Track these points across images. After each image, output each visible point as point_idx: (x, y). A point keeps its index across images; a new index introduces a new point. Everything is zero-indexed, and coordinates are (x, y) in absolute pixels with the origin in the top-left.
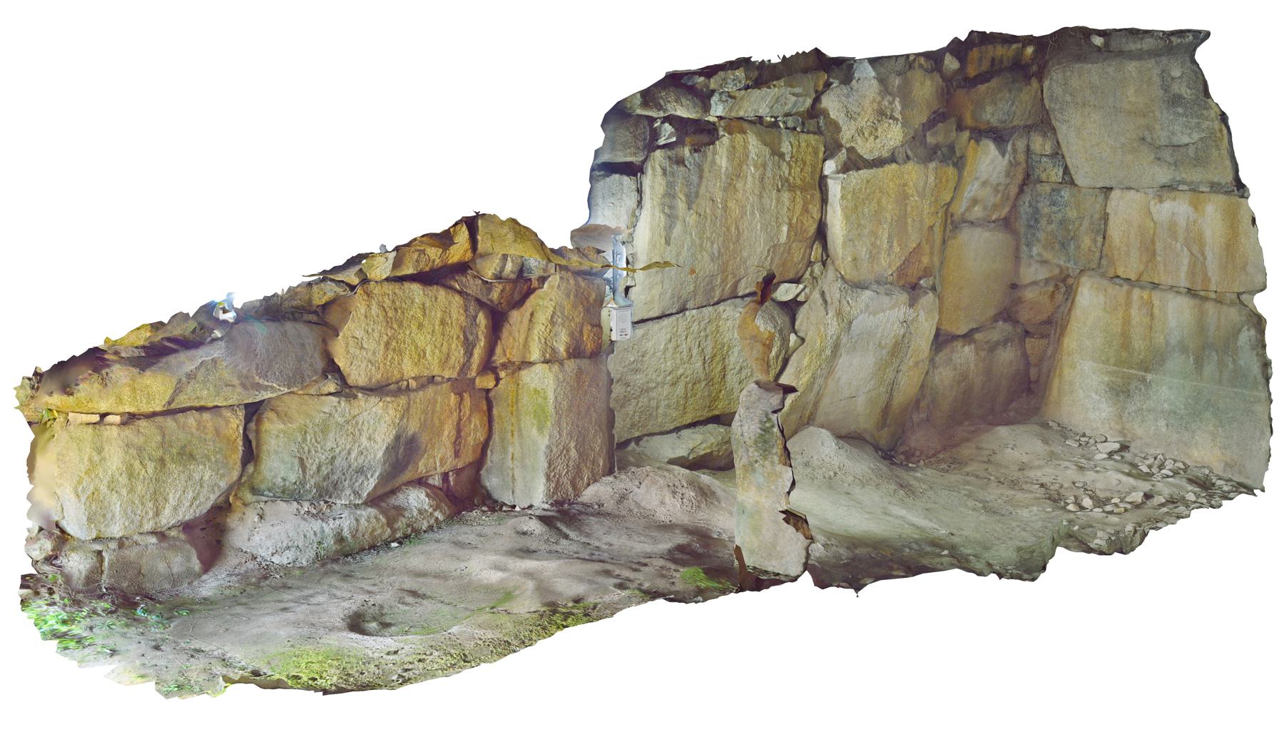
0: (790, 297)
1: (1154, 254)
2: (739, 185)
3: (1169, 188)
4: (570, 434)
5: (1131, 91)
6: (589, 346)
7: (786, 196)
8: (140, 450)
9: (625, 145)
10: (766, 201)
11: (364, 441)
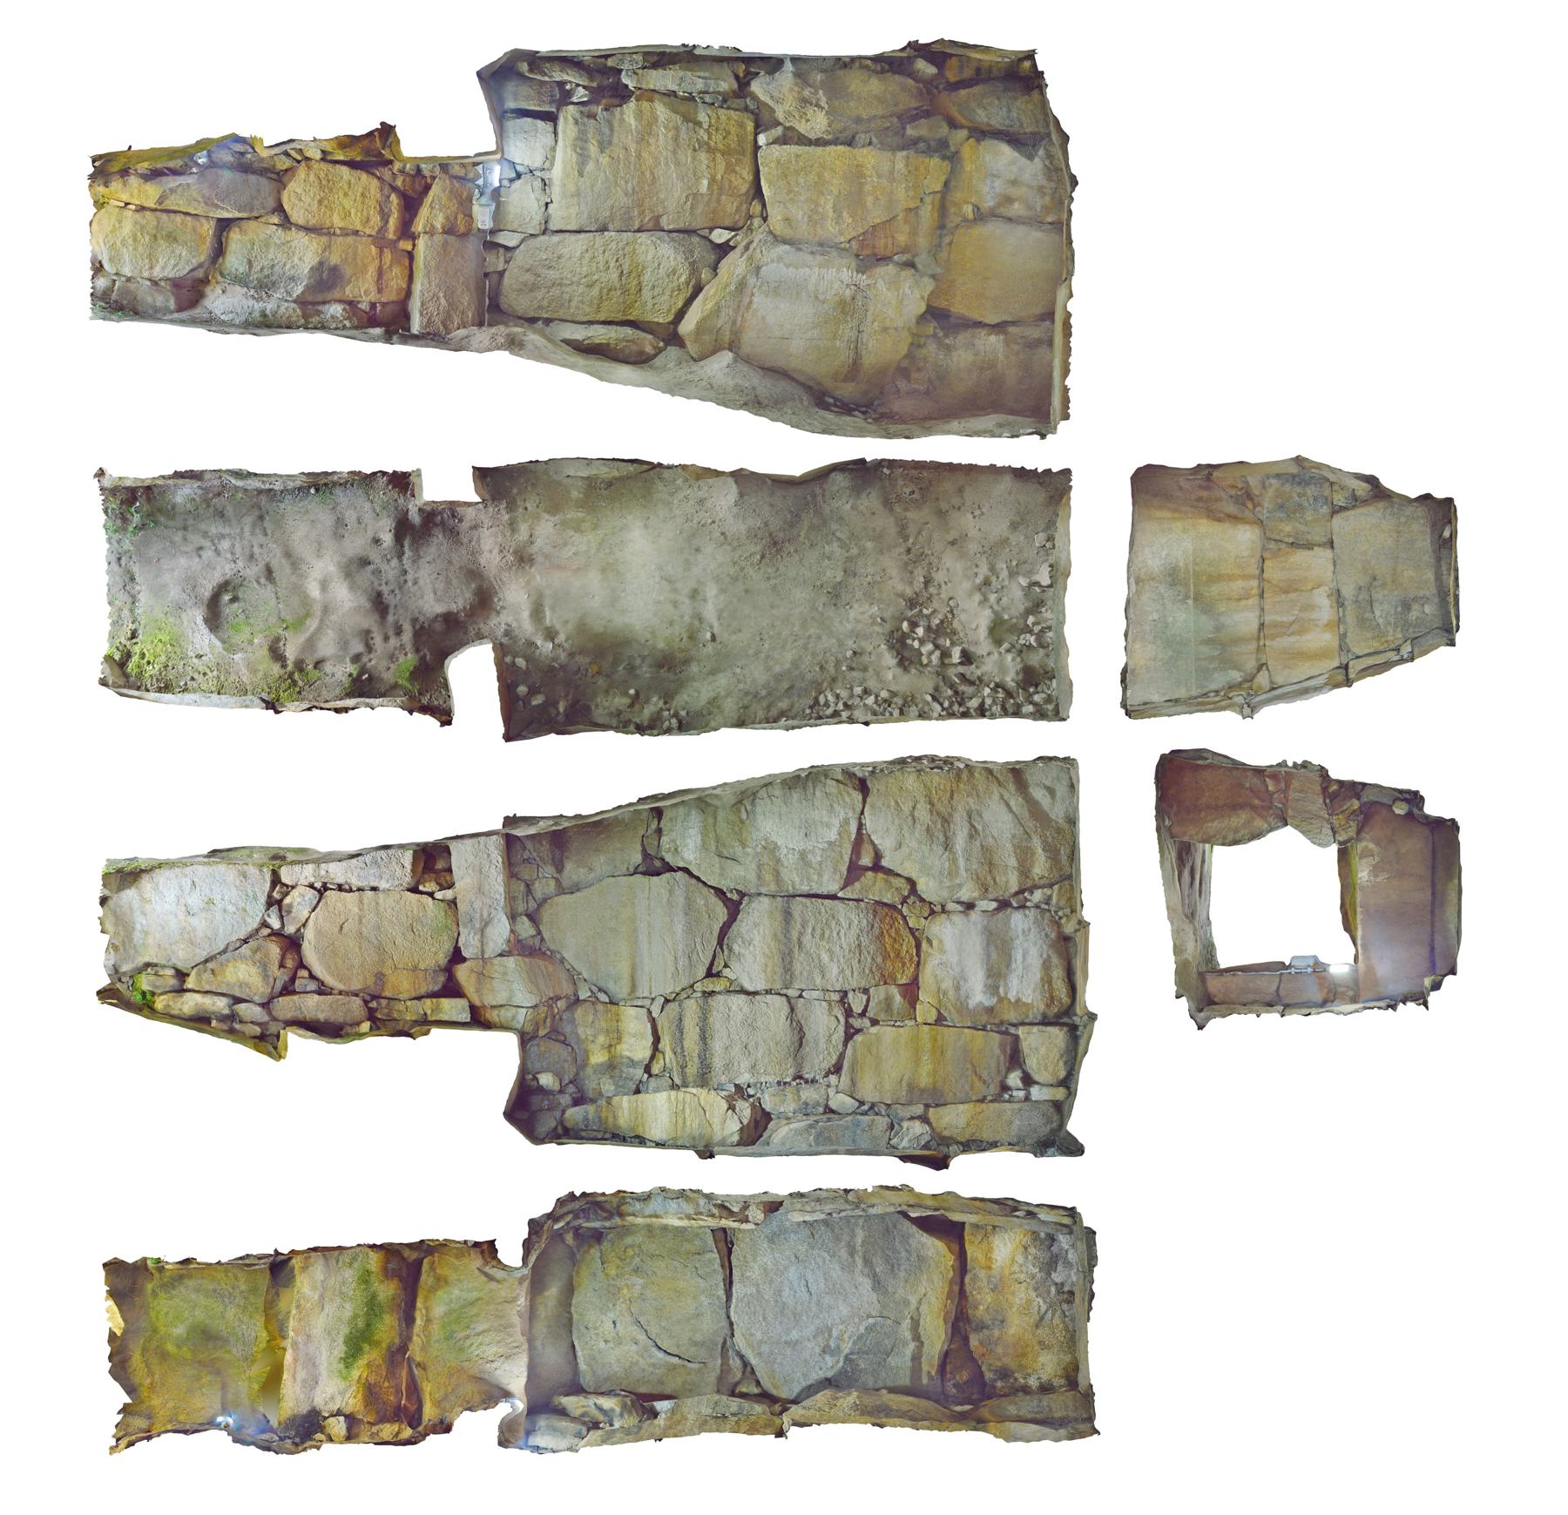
0: (720, 241)
1: (1286, 592)
2: (652, 141)
3: (1338, 598)
4: (438, 286)
5: (1411, 573)
6: (462, 229)
7: (703, 156)
8: (142, 227)
9: (528, 98)
10: (680, 155)
11: (296, 260)
